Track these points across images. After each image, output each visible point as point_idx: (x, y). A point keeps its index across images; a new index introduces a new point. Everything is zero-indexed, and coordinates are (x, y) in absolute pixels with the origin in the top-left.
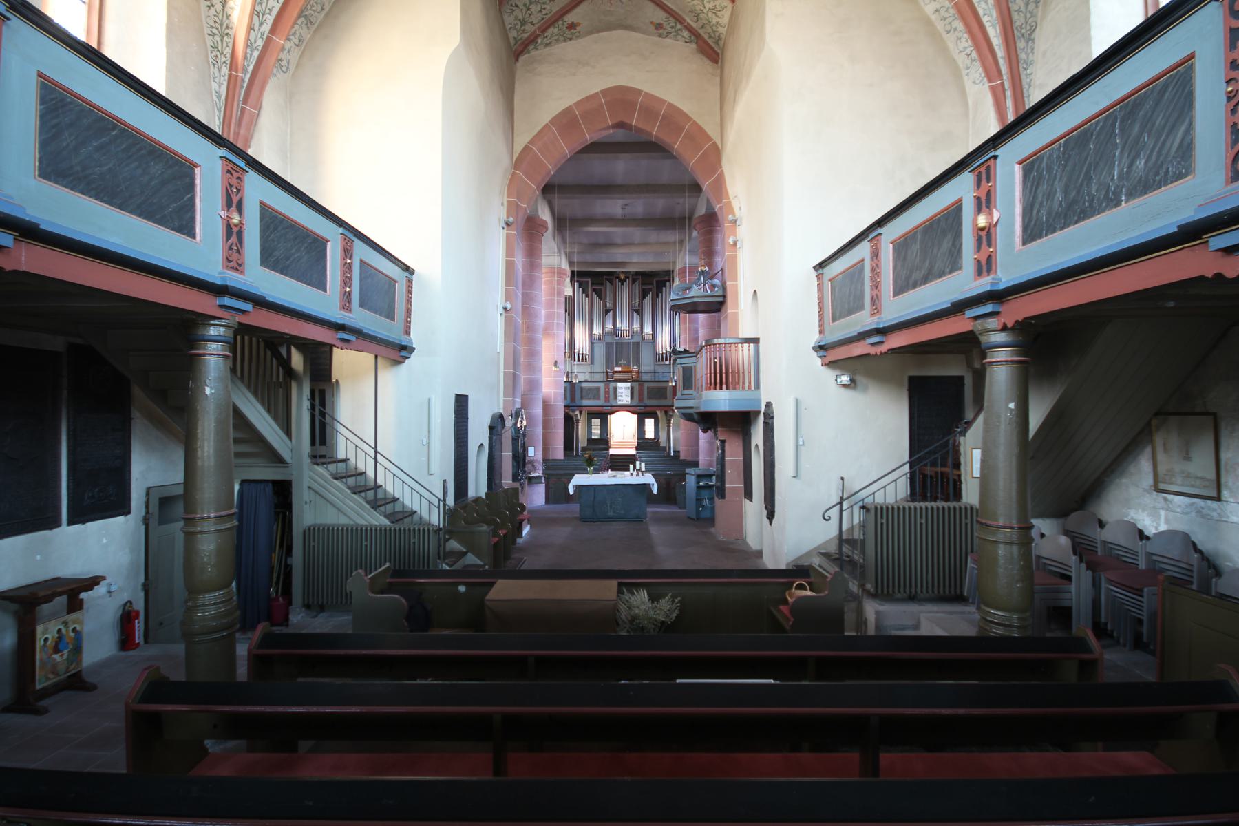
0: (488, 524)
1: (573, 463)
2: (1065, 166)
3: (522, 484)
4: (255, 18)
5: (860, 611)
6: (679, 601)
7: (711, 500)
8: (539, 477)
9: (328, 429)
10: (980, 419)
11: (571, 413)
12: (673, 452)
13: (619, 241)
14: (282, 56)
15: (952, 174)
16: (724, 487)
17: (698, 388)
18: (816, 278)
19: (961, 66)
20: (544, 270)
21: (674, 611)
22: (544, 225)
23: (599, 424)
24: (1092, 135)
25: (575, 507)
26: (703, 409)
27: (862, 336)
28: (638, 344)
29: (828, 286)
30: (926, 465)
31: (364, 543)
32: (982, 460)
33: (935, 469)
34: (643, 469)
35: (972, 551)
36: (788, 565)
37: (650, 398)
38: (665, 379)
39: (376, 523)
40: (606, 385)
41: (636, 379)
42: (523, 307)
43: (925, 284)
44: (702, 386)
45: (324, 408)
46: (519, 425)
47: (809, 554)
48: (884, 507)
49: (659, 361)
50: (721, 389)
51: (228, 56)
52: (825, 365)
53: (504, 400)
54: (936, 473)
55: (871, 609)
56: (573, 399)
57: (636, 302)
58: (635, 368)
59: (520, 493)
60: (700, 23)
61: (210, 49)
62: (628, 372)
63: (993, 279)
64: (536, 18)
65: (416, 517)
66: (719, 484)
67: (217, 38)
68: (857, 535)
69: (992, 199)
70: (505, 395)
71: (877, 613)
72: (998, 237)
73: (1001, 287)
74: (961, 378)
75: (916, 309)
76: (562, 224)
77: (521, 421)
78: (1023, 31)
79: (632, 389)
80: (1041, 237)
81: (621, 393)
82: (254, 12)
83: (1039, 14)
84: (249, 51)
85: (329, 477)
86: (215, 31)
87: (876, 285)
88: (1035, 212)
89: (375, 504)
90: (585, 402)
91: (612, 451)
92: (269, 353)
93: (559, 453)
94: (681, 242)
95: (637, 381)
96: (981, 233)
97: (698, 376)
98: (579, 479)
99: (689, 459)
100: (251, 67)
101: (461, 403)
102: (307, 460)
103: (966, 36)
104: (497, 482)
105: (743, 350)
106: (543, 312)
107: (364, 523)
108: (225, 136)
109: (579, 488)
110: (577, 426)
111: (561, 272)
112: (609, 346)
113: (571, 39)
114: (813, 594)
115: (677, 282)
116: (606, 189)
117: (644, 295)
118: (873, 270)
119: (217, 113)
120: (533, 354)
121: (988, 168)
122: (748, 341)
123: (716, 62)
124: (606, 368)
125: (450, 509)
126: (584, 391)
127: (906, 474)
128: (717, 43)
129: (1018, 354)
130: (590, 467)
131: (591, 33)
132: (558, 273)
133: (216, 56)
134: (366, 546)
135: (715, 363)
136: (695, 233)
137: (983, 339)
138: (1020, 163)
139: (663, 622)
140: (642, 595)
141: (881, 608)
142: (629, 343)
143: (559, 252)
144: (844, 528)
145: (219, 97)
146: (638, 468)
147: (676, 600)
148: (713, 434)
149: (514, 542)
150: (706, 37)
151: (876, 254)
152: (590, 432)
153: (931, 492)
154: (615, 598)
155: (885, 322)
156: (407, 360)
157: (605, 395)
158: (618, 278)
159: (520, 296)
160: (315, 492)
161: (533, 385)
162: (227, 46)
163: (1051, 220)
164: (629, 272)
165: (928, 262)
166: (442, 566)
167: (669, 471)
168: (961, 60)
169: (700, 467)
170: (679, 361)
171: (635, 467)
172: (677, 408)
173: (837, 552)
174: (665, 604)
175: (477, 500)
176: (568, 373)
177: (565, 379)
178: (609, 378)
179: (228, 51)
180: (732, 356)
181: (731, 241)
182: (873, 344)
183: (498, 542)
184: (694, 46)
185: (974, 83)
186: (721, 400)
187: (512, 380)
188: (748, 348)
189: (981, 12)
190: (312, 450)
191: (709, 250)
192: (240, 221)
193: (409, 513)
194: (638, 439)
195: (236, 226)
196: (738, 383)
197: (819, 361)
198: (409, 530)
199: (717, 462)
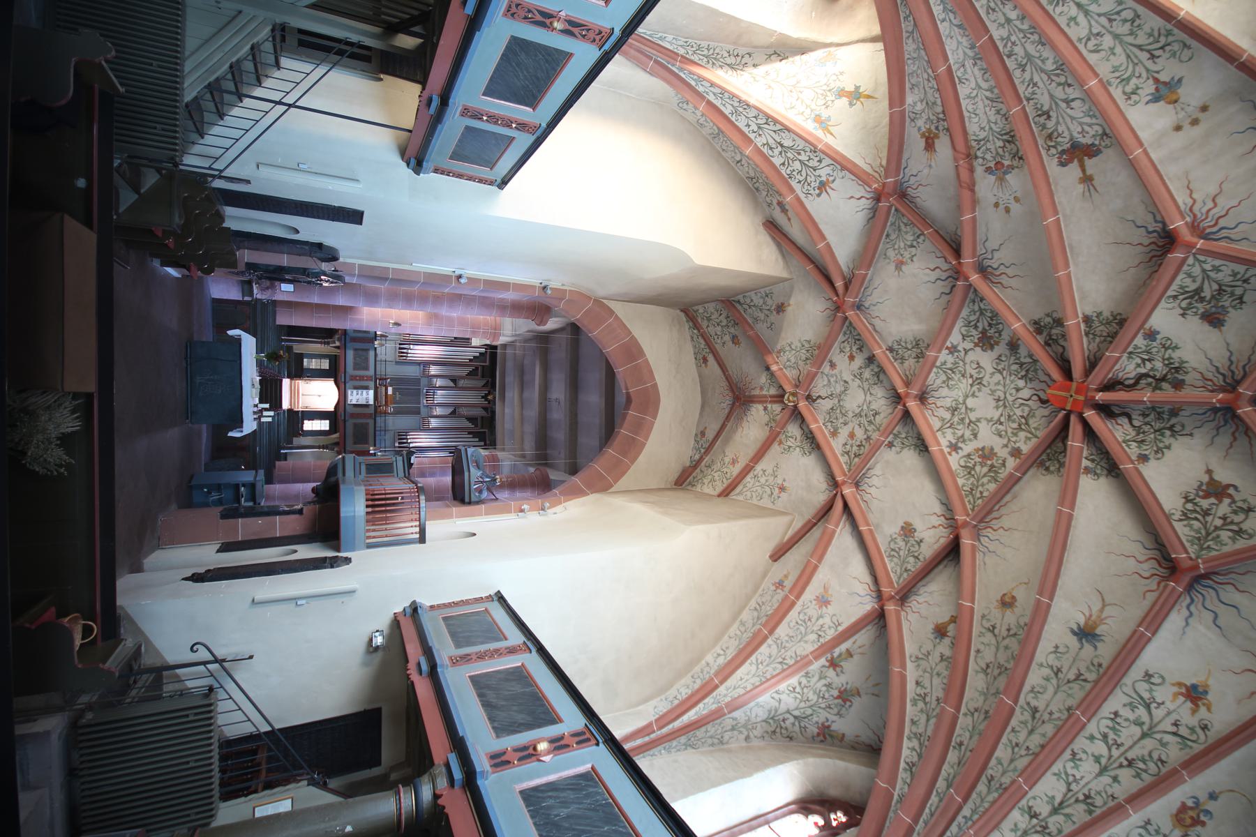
2: (589, 810)
3: (242, 273)
4: (719, 91)
5: (48, 711)
6: (60, 474)
7: (220, 502)
8: (251, 294)
9: (322, 54)
10: (329, 798)
11: (337, 336)
12: (286, 453)
13: (526, 394)
14: (691, 106)
15: (583, 707)
16: (239, 517)
17: (368, 481)
18: (488, 595)
19: (667, 694)
20: (498, 318)
21: (43, 468)
22: (542, 322)
23: (323, 368)
24: (615, 825)
25: (208, 335)
26: (342, 487)
27: (428, 652)
28: (418, 412)
29: (480, 608)
30: (270, 750)
31: (155, 63)
32: (279, 814)
33: (264, 762)
34: (263, 420)
35: (148, 831)
36: (122, 608)
37: (355, 425)
38: (377, 442)
39: (185, 85)
40: (371, 377)
41: (379, 410)
42: (461, 295)
43: (483, 705)
44: (371, 485)
45: (349, 57)
46: (322, 277)
47: (138, 631)
48: (212, 714)
50: (367, 506)
51: (692, 58)
52: (395, 617)
54: (259, 764)
55: (54, 725)
56: (354, 340)
57: (464, 411)
59: (229, 270)
60: (704, 469)
61: (699, 42)
62: (386, 402)
63: (487, 771)
64: (711, 330)
65: (194, 136)
67: (705, 52)
68: (168, 688)
69: (561, 751)
70: (360, 266)
71: (47, 734)
72: (528, 765)
73: (480, 782)
74: (378, 763)
75: (457, 701)
76: (543, 340)
77: (328, 281)
78: (692, 739)
79: (367, 406)
80: (527, 806)
81: (362, 394)
82: (724, 91)
83: (704, 749)
84: (695, 77)
85: (255, 41)
86: (711, 51)
87: (481, 657)
88: (550, 794)
89: (214, 88)
90: (350, 354)
91: (286, 382)
92: (416, 13)
93: (283, 319)
94: (523, 456)
95: (376, 410)
96: (531, 748)
98: (249, 344)
99: (276, 472)
100: (683, 76)
101: (354, 217)
102: (280, 19)
103: (690, 692)
104: (246, 243)
107: (187, 69)
108: (633, 36)
109: (237, 342)
110: (321, 343)
111: (496, 335)
112: (417, 381)
113: (696, 358)
114: (77, 649)
115: (484, 453)
116: (575, 385)
117: (470, 419)
118: (497, 651)
119: (649, 33)
120: (409, 300)
121: (588, 740)
122: (422, 532)
123: (676, 484)
125: (206, 182)
127: (258, 730)
128: (690, 484)
129: (409, 819)
130: (266, 356)
131: (700, 376)
133: (692, 47)
134: (151, 65)
136: (532, 470)
137: (425, 778)
138: (593, 768)
139: (24, 453)
140: (71, 425)
141: (55, 737)
143: (516, 335)
144: (178, 671)
145: (660, 39)
146: (265, 413)
147: (62, 470)
148: (310, 500)
149: (157, 256)
150: (694, 474)
151: (512, 651)
153: (232, 764)
154: (67, 389)
155: (443, 672)
156: (404, 164)
157: (360, 376)
158: (489, 393)
159: (473, 294)
160: (234, 18)
161: (372, 298)
163: (543, 811)
164: (495, 404)
165: (503, 703)
166: (117, 158)
167: (260, 449)
168: (672, 693)
170: (399, 459)
171: (266, 410)
172: (343, 458)
173: (142, 667)
174: (57, 455)
175: (221, 218)
177: (378, 333)
178: (379, 382)
179: (695, 58)
180: (406, 515)
181: (525, 507)
182: (419, 664)
184: (688, 464)
185: (655, 707)
186: (354, 507)
187: (380, 276)
189: (706, 701)
190: (293, 28)
191: (514, 485)
192: (556, 29)
193: (201, 130)
195: (551, 23)
197: (399, 609)
198: (176, 126)
199: (273, 506)
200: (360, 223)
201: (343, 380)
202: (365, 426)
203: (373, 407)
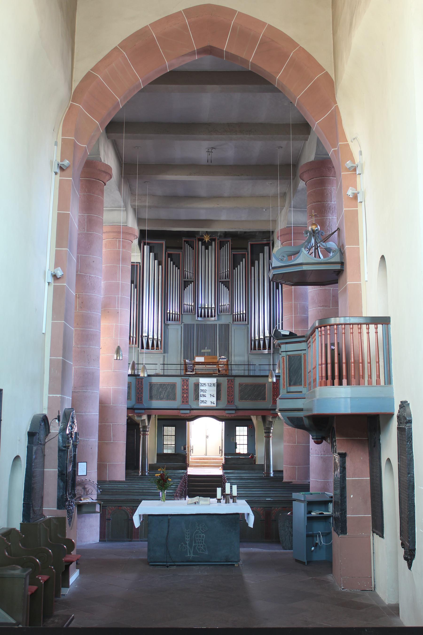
0: (24, 566)
1: (138, 486)
3: (70, 512)
7: (327, 535)
8: (93, 505)
11: (136, 418)
12: (274, 471)
13: (203, 193)
17: (310, 384)
20: (105, 229)
22: (107, 172)
26: (316, 411)
28: (226, 328)
34: (235, 493)
37: (242, 398)
41: (224, 372)
44: (315, 380)
49: (255, 349)
50: (341, 384)
53: (49, 397)
56: (139, 399)
57: (225, 270)
58: (223, 359)
62: (214, 364)
66: (338, 514)
70: (50, 392)
79: (219, 386)
90: (156, 404)
91: (191, 471)
94: (283, 195)
97: (310, 367)
99: (296, 481)
105: (368, 333)
106: (103, 284)
110: (144, 435)
115: (278, 246)
124: (184, 358)
132: (123, 232)
135: (333, 350)
136: (302, 184)
142: (215, 325)
143: (126, 206)
146: (228, 491)
148: (330, 446)
149: (58, 593)
152: (160, 444)
159: (75, 260)
169: (311, 491)
170: (284, 347)
171: (223, 491)
172: (280, 410)
176: (134, 364)
177: (130, 372)
181: (350, 192)
183: (36, 591)
188: (374, 330)
194: (225, 455)
196: (363, 377)
201: (188, 411)
202: (243, 388)
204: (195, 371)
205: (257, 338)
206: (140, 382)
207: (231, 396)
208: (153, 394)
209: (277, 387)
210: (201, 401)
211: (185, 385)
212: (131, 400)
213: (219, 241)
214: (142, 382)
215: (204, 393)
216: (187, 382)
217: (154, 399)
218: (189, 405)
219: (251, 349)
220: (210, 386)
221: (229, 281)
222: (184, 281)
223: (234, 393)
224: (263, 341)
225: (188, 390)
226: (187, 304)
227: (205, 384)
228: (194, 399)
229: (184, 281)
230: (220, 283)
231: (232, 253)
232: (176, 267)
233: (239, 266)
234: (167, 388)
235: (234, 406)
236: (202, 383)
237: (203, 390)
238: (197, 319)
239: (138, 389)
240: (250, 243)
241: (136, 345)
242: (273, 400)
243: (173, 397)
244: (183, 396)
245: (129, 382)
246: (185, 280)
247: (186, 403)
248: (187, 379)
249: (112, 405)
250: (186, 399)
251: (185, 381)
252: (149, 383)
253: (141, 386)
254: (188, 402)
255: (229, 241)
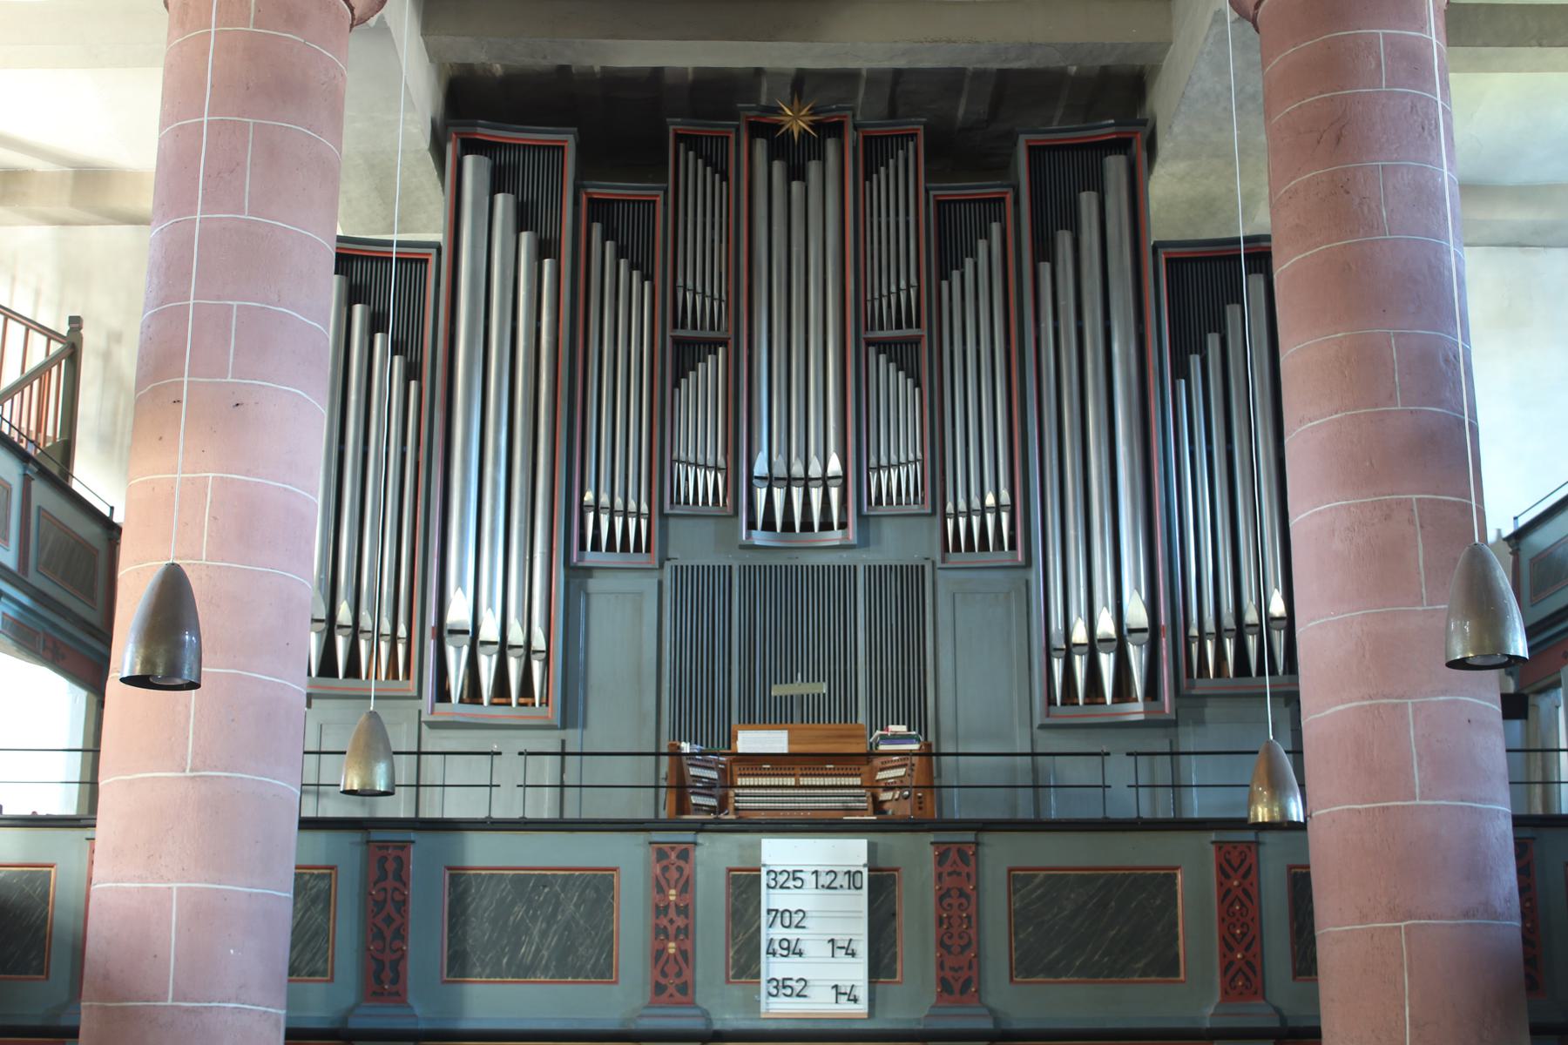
37: (1026, 965)
41: (905, 810)
49: (957, 548)
62: (845, 762)
126: (482, 908)
142: (848, 572)
162: (882, 763)
164: (848, 78)
200: (70, 317)
203: (878, 838)
204: (737, 809)
205: (1079, 635)
206: (391, 866)
207: (961, 952)
208: (470, 941)
209: (1244, 890)
210: (769, 981)
211: (672, 883)
212: (332, 980)
213: (861, 135)
214: (402, 864)
215: (792, 934)
216: (681, 863)
217: (478, 970)
218: (698, 1012)
219: (1051, 701)
220: (829, 887)
221: (915, 342)
222: (677, 342)
223: (978, 933)
224: (1112, 655)
225: (690, 913)
226: (691, 458)
227: (794, 875)
228: (731, 973)
229: (677, 342)
230: (872, 350)
231: (932, 193)
232: (631, 267)
233: (969, 262)
234: (557, 905)
235: (984, 1011)
236: (778, 869)
237: (787, 914)
238: (749, 536)
239: (380, 905)
240: (1027, 141)
241: (407, 682)
242: (1225, 971)
243: (598, 960)
244: (659, 954)
245: (309, 862)
246: (680, 333)
247: (677, 995)
248: (684, 846)
249: (169, 1003)
250: (679, 974)
251: (673, 856)
252: (449, 868)
253: (396, 889)
254: (690, 991)
255: (913, 136)
